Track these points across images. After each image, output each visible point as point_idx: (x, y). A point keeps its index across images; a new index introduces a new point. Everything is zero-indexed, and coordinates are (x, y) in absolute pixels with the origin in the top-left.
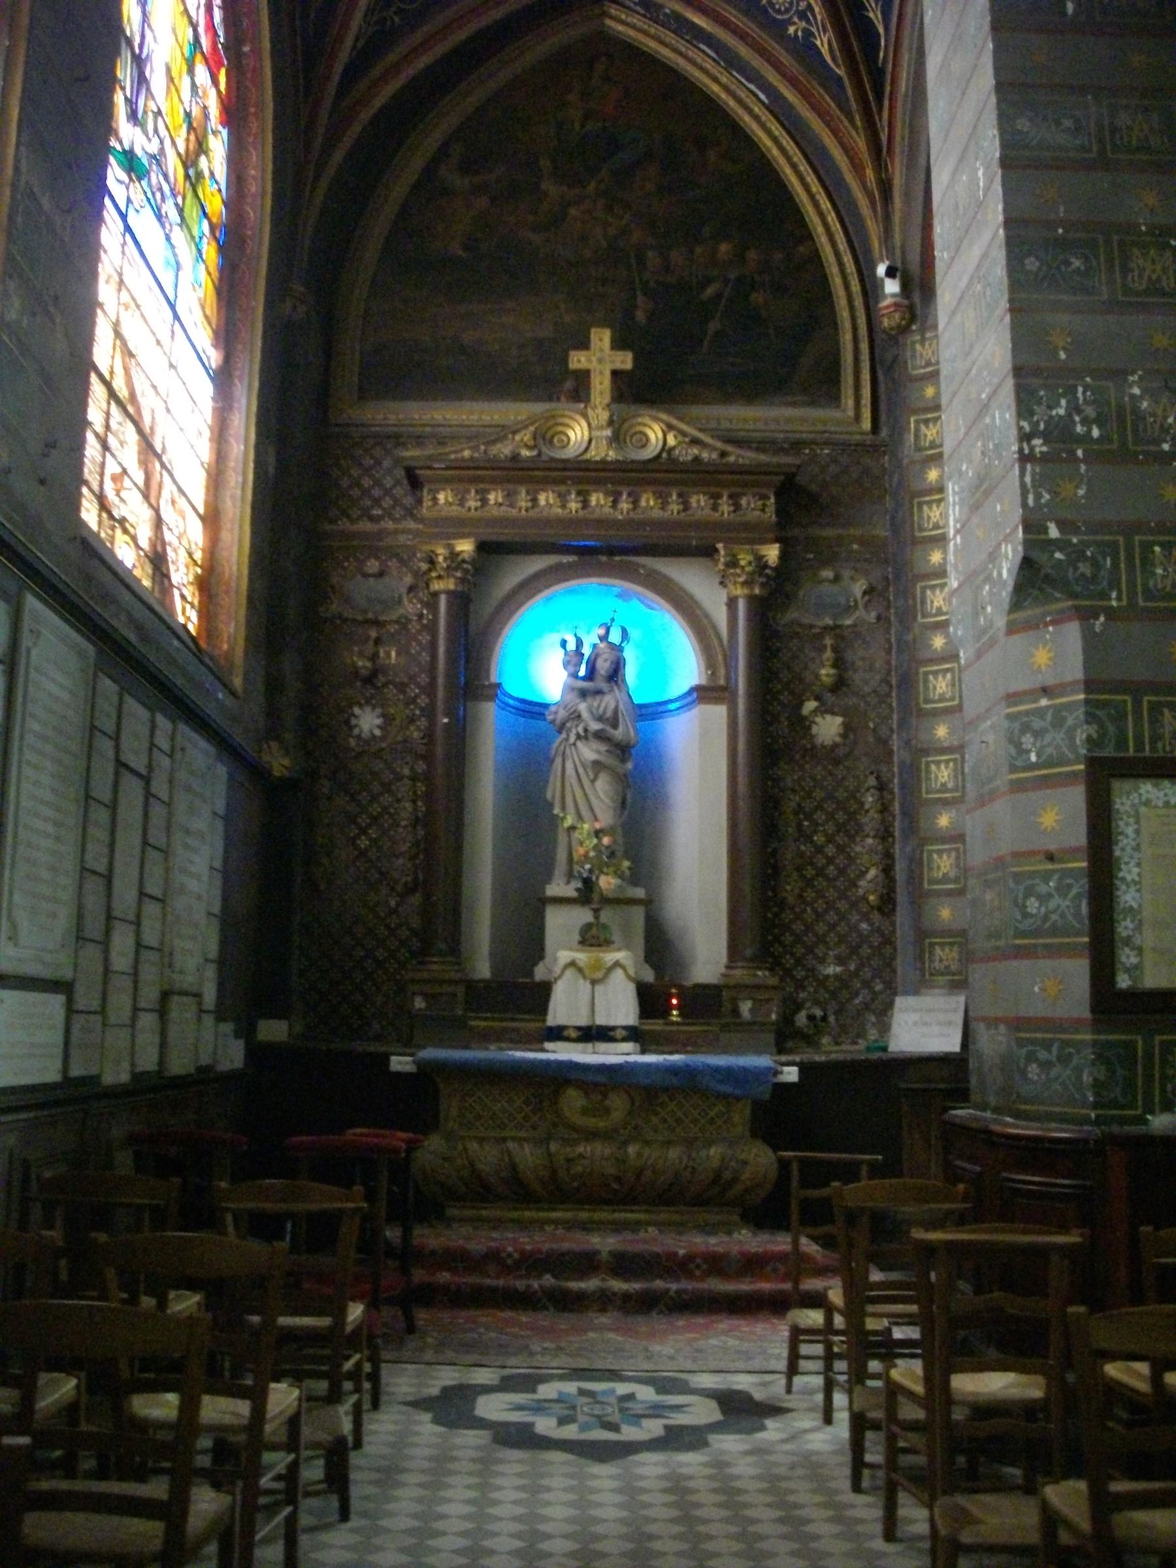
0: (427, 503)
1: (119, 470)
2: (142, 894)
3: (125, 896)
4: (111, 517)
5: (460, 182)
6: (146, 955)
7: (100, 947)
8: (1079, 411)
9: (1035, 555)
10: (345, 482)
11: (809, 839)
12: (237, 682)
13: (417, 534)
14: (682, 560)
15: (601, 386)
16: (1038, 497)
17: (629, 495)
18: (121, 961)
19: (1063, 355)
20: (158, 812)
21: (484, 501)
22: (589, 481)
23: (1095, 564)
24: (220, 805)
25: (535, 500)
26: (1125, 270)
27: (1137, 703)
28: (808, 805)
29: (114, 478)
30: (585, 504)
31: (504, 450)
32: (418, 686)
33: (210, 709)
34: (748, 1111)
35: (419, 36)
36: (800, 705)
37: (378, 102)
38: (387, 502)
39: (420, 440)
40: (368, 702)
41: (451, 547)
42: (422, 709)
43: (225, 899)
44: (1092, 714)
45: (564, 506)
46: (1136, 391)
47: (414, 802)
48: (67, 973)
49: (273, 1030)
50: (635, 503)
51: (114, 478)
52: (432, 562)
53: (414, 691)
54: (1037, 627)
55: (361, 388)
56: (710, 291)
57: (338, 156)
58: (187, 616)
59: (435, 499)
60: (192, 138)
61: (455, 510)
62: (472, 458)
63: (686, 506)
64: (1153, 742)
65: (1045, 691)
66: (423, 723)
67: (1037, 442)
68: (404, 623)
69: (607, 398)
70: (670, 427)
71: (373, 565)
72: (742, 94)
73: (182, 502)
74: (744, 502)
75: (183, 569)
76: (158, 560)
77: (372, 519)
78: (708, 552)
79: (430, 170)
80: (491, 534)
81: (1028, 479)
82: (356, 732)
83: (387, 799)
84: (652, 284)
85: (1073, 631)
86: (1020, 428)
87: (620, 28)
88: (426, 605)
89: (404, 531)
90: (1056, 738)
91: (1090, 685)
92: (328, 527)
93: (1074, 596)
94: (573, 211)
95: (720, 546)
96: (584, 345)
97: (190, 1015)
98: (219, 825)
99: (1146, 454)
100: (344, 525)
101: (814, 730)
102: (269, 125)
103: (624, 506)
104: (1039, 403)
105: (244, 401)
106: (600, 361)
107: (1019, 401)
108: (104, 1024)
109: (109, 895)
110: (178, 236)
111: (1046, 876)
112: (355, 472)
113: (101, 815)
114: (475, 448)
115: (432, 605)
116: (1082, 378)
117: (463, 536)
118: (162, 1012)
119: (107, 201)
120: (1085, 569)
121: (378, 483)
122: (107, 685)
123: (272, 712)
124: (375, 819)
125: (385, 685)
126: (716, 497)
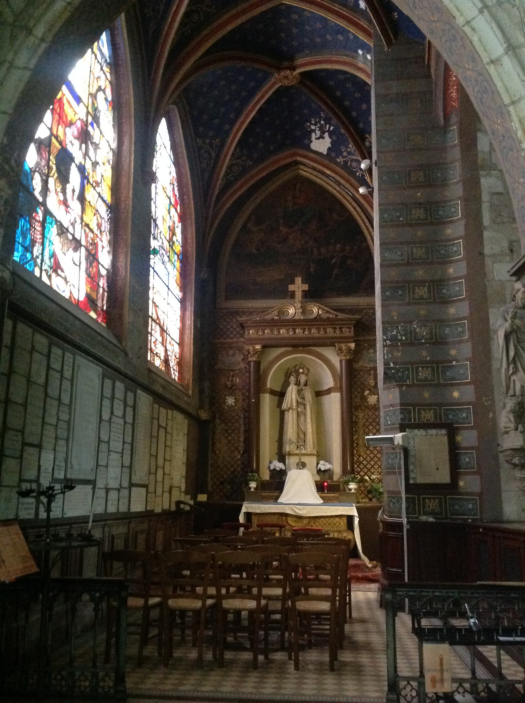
0: (246, 333)
1: (155, 339)
2: (165, 459)
3: (160, 461)
4: (153, 354)
6: (166, 476)
7: (66, 423)
8: (400, 333)
9: (387, 371)
10: (222, 327)
12: (190, 392)
14: (325, 348)
15: (299, 295)
16: (388, 356)
17: (308, 329)
18: (159, 478)
19: (395, 318)
20: (169, 436)
21: (264, 333)
23: (403, 372)
24: (186, 431)
25: (279, 332)
26: (414, 293)
27: (414, 409)
29: (154, 342)
31: (268, 317)
34: (346, 521)
36: (364, 392)
37: (228, 206)
38: (235, 333)
39: (244, 313)
40: (230, 394)
41: (254, 348)
42: (247, 396)
43: (188, 459)
44: (402, 411)
46: (415, 326)
48: (147, 483)
49: (202, 498)
51: (154, 342)
52: (249, 352)
53: (244, 391)
54: (389, 389)
55: (226, 296)
56: (334, 261)
57: (216, 225)
58: (175, 375)
60: (171, 232)
62: (260, 320)
63: (326, 332)
64: (419, 419)
65: (392, 405)
67: (388, 341)
69: (300, 299)
70: (320, 308)
72: (344, 193)
73: (173, 342)
74: (344, 330)
75: (173, 361)
76: (166, 361)
77: (230, 338)
78: (333, 345)
79: (244, 226)
81: (385, 352)
82: (227, 404)
83: (236, 424)
85: (397, 391)
86: (384, 338)
87: (304, 173)
91: (401, 404)
92: (217, 341)
93: (396, 382)
94: (290, 237)
95: (336, 344)
96: (293, 282)
97: (178, 493)
98: (186, 437)
99: (418, 343)
100: (222, 340)
101: (368, 400)
102: (194, 221)
103: (307, 333)
104: (389, 331)
105: (190, 308)
106: (298, 288)
107: (383, 331)
108: (155, 496)
109: (157, 461)
110: (169, 265)
111: (393, 454)
112: (225, 323)
113: (154, 440)
114: (261, 317)
115: (250, 366)
116: (400, 324)
118: (170, 493)
120: (400, 374)
121: (232, 327)
122: (156, 406)
123: (201, 400)
124: (233, 431)
125: (236, 389)
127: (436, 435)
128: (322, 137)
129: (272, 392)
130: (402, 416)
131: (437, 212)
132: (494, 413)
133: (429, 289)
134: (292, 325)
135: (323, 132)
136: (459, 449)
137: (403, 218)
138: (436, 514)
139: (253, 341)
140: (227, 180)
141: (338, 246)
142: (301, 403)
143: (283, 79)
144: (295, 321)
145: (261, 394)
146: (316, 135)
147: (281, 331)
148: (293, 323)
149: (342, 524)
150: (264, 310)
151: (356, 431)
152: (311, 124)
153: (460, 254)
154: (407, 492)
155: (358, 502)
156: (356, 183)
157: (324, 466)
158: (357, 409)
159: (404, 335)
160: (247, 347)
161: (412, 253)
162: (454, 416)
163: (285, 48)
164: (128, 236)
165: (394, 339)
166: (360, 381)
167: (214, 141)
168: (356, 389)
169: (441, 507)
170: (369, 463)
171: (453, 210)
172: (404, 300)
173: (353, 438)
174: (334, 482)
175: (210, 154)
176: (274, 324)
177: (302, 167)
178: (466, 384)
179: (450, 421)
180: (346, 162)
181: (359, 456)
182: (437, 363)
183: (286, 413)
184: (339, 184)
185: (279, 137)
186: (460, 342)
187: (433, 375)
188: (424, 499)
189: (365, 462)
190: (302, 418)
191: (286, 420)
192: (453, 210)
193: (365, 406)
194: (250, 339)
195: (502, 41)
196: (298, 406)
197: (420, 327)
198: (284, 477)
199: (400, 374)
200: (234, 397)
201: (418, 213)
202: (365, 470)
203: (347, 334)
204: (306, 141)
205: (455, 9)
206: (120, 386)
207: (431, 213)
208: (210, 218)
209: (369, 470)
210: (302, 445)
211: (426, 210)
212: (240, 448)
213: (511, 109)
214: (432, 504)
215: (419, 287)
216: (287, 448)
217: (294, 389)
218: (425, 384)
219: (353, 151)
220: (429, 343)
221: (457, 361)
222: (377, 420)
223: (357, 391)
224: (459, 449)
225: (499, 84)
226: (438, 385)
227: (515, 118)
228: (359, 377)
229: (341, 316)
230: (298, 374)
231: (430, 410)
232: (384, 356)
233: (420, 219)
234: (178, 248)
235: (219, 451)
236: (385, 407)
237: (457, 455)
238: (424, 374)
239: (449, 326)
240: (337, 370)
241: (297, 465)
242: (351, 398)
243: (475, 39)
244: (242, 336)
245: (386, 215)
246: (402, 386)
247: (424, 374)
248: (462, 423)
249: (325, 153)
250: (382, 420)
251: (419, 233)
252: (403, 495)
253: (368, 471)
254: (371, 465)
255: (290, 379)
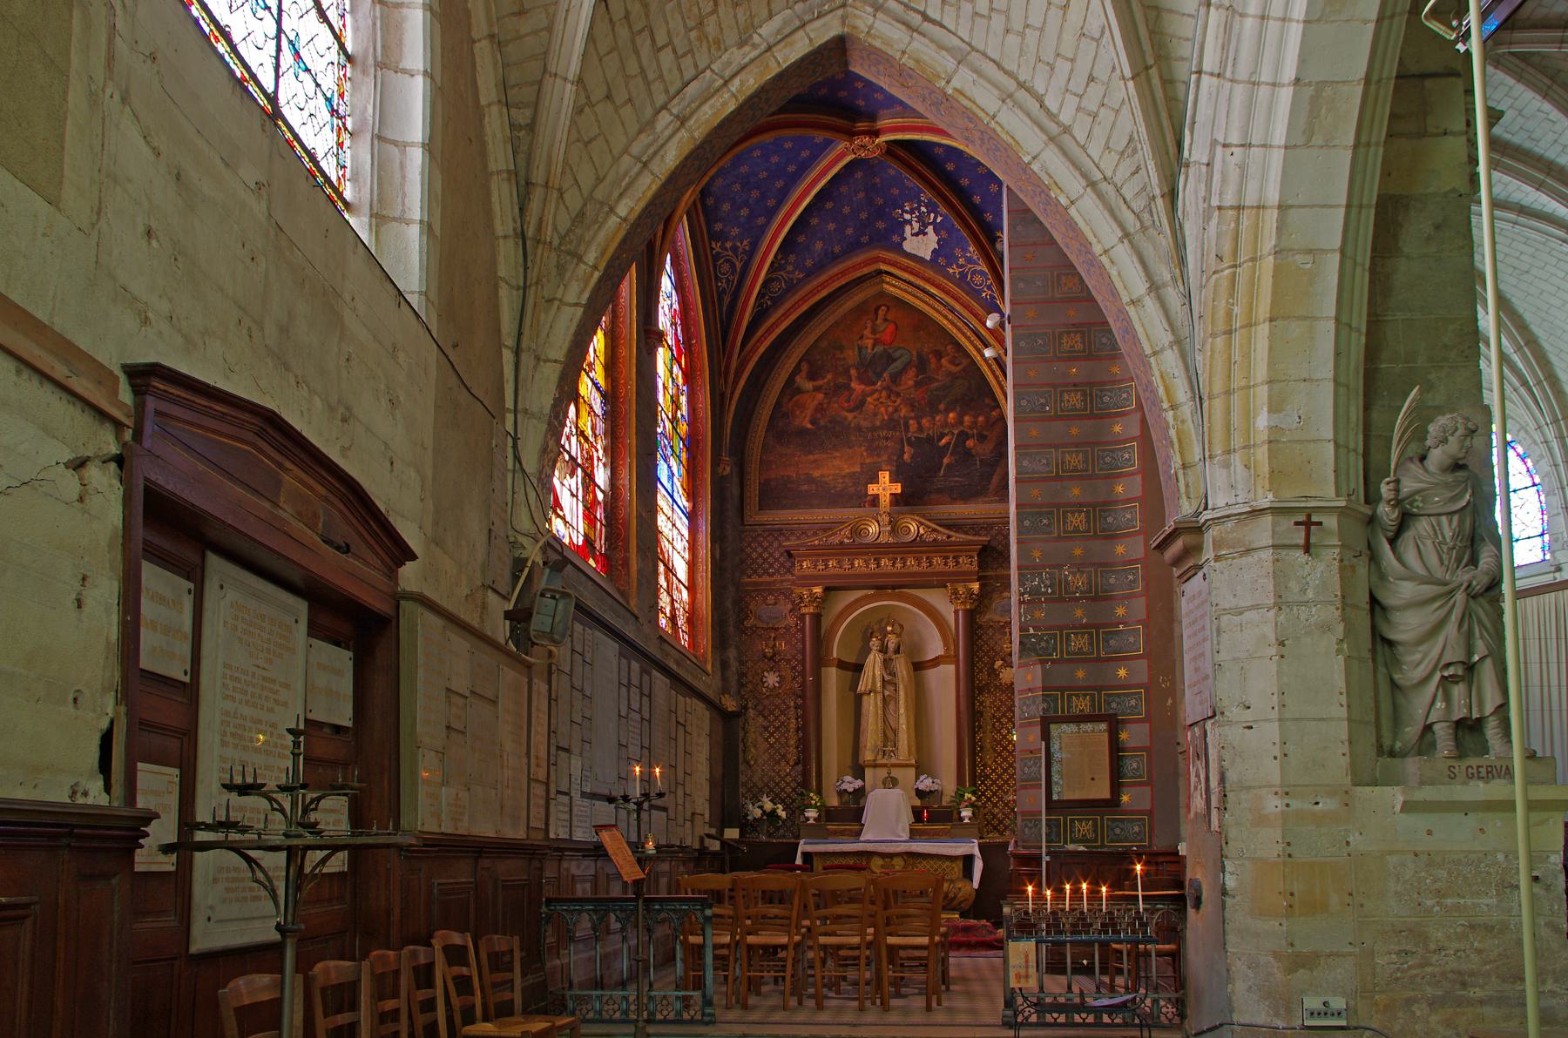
5: (809, 385)
9: (1024, 640)
11: (999, 732)
12: (709, 668)
13: (793, 583)
16: (1026, 617)
21: (827, 566)
22: (880, 553)
23: (1047, 641)
25: (853, 564)
28: (998, 715)
30: (878, 565)
31: (835, 540)
32: (796, 660)
33: (701, 687)
35: (781, 312)
38: (776, 565)
40: (772, 670)
45: (867, 567)
47: (797, 719)
50: (904, 563)
53: (794, 663)
57: (742, 383)
59: (801, 565)
61: (812, 571)
66: (800, 679)
68: (787, 628)
70: (921, 524)
71: (771, 599)
76: (673, 619)
79: (791, 379)
80: (829, 582)
82: (766, 685)
84: (913, 439)
88: (798, 618)
89: (785, 581)
90: (1033, 708)
94: (869, 399)
96: (875, 480)
107: (1019, 580)
111: (1030, 759)
115: (803, 621)
117: (816, 585)
119: (659, 486)
120: (1043, 644)
121: (771, 555)
123: (724, 679)
125: (780, 660)
126: (946, 558)
127: (1093, 731)
128: (922, 232)
129: (842, 665)
130: (1045, 705)
131: (1101, 398)
132: (1174, 699)
133: (1088, 517)
134: (873, 553)
135: (925, 225)
136: (1124, 750)
137: (1051, 408)
138: (1088, 841)
139: (809, 581)
140: (761, 305)
141: (951, 415)
142: (889, 682)
143: (859, 149)
144: (880, 546)
145: (823, 669)
146: (912, 229)
147: (856, 563)
148: (876, 550)
149: (956, 869)
150: (828, 527)
151: (980, 727)
152: (903, 211)
153: (1133, 465)
154: (1048, 813)
155: (981, 838)
156: (980, 311)
157: (926, 783)
158: (981, 690)
159: (1050, 586)
160: (798, 590)
161: (1063, 463)
162: (1118, 704)
163: (861, 103)
164: (631, 439)
165: (1035, 592)
166: (988, 645)
167: (739, 244)
168: (980, 659)
169: (1095, 831)
170: (1000, 776)
171: (1124, 395)
172: (1050, 533)
173: (974, 738)
174: (944, 807)
175: (733, 266)
176: (841, 550)
177: (888, 279)
178: (1137, 657)
179: (1111, 712)
180: (963, 276)
181: (985, 766)
182: (1097, 627)
183: (865, 698)
184: (952, 310)
185: (849, 231)
186: (1129, 597)
187: (1091, 644)
188: (1072, 821)
189: (993, 776)
190: (891, 707)
191: (864, 710)
192: (1124, 395)
193: (996, 686)
194: (804, 577)
195: (1144, 279)
196: (884, 687)
197: (1074, 574)
198: (861, 801)
199: (1043, 644)
200: (777, 674)
201: (1074, 400)
202: (994, 788)
203: (966, 568)
204: (895, 238)
205: (1091, 234)
206: (635, 666)
207: (1091, 400)
208: (732, 371)
209: (1000, 788)
210: (892, 751)
211: (1084, 394)
212: (789, 756)
213: (1152, 360)
214: (1084, 827)
215: (1073, 513)
216: (868, 756)
217: (878, 659)
218: (1078, 659)
219: (975, 257)
220: (1087, 598)
221: (1125, 624)
222: (1009, 715)
223: (983, 662)
224: (1124, 750)
225: (1140, 330)
226: (1099, 660)
227: (1156, 373)
228: (985, 638)
229: (957, 537)
230: (885, 634)
231: (1085, 695)
232: (1020, 619)
233: (1076, 410)
234: (683, 428)
235: (756, 761)
236: (1021, 692)
237: (1120, 758)
238: (1078, 643)
239: (1114, 572)
240: (949, 626)
241: (884, 784)
242: (972, 671)
243: (1114, 273)
244: (789, 571)
245: (1024, 403)
246: (1046, 661)
247: (1078, 643)
248: (1130, 714)
249: (928, 258)
250: (1017, 710)
251: (1074, 431)
252: (1044, 817)
253: (761, 556)
254: (1003, 780)
255: (871, 643)
